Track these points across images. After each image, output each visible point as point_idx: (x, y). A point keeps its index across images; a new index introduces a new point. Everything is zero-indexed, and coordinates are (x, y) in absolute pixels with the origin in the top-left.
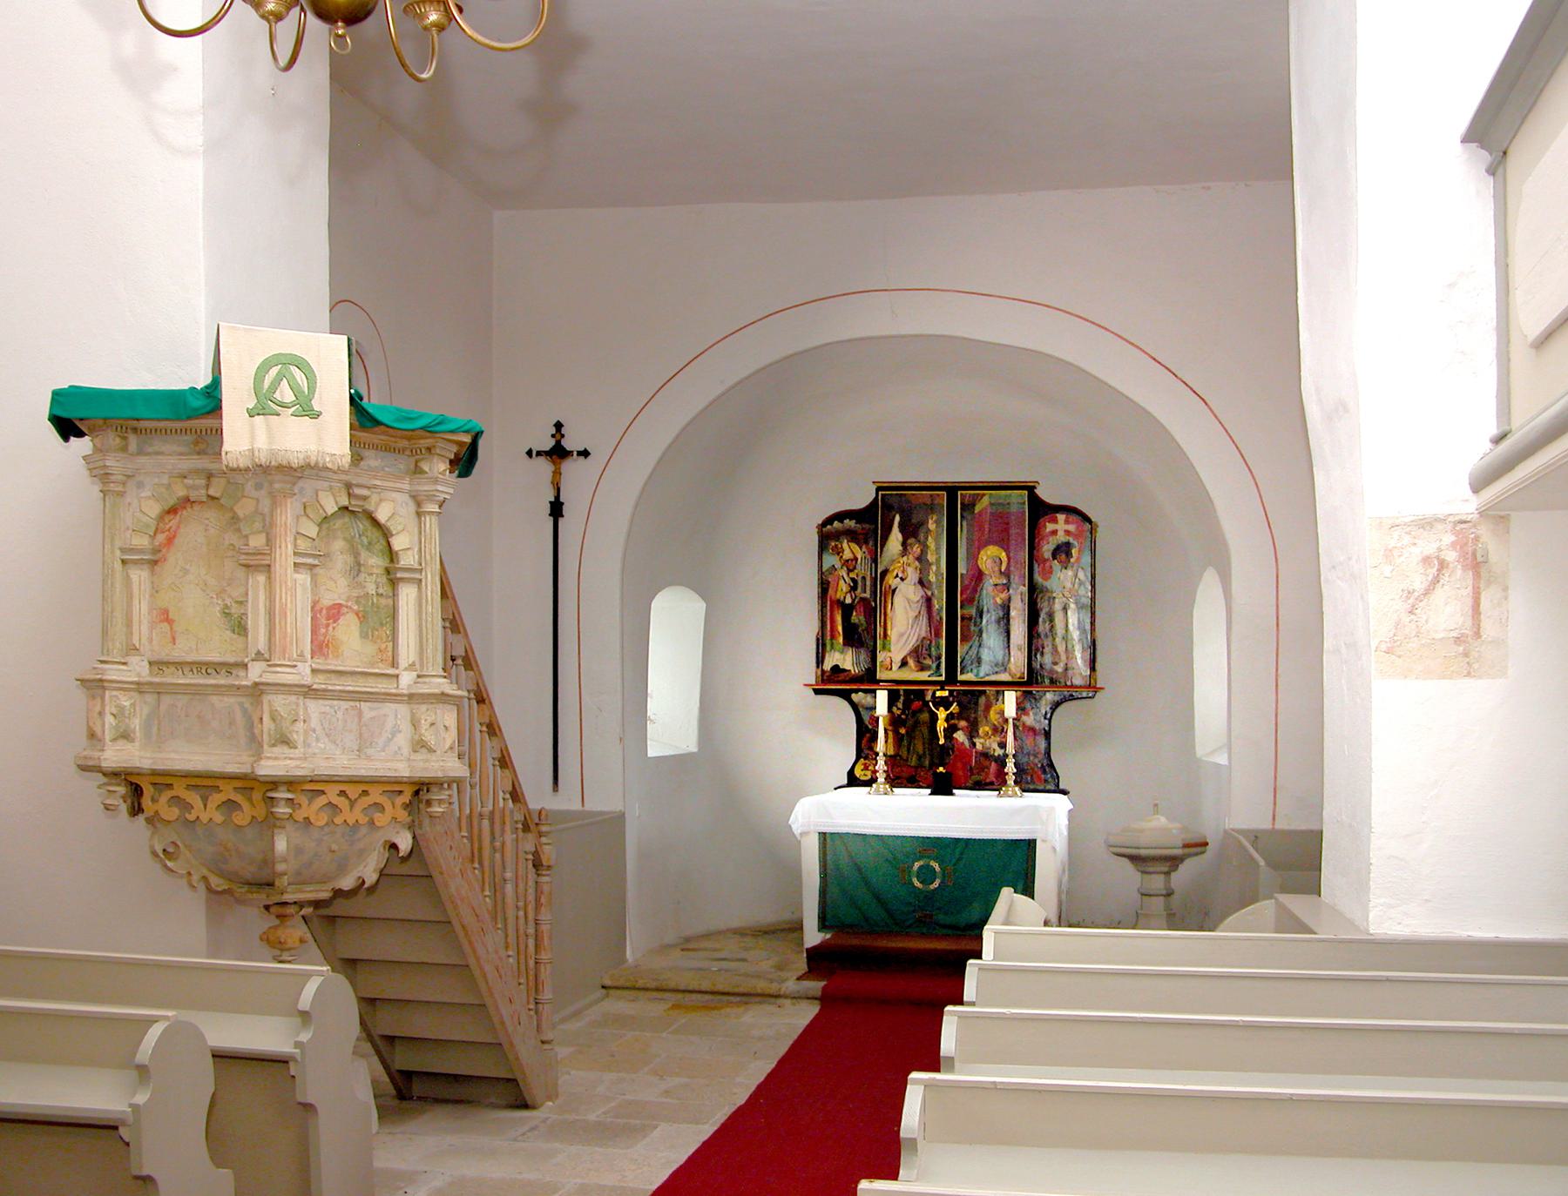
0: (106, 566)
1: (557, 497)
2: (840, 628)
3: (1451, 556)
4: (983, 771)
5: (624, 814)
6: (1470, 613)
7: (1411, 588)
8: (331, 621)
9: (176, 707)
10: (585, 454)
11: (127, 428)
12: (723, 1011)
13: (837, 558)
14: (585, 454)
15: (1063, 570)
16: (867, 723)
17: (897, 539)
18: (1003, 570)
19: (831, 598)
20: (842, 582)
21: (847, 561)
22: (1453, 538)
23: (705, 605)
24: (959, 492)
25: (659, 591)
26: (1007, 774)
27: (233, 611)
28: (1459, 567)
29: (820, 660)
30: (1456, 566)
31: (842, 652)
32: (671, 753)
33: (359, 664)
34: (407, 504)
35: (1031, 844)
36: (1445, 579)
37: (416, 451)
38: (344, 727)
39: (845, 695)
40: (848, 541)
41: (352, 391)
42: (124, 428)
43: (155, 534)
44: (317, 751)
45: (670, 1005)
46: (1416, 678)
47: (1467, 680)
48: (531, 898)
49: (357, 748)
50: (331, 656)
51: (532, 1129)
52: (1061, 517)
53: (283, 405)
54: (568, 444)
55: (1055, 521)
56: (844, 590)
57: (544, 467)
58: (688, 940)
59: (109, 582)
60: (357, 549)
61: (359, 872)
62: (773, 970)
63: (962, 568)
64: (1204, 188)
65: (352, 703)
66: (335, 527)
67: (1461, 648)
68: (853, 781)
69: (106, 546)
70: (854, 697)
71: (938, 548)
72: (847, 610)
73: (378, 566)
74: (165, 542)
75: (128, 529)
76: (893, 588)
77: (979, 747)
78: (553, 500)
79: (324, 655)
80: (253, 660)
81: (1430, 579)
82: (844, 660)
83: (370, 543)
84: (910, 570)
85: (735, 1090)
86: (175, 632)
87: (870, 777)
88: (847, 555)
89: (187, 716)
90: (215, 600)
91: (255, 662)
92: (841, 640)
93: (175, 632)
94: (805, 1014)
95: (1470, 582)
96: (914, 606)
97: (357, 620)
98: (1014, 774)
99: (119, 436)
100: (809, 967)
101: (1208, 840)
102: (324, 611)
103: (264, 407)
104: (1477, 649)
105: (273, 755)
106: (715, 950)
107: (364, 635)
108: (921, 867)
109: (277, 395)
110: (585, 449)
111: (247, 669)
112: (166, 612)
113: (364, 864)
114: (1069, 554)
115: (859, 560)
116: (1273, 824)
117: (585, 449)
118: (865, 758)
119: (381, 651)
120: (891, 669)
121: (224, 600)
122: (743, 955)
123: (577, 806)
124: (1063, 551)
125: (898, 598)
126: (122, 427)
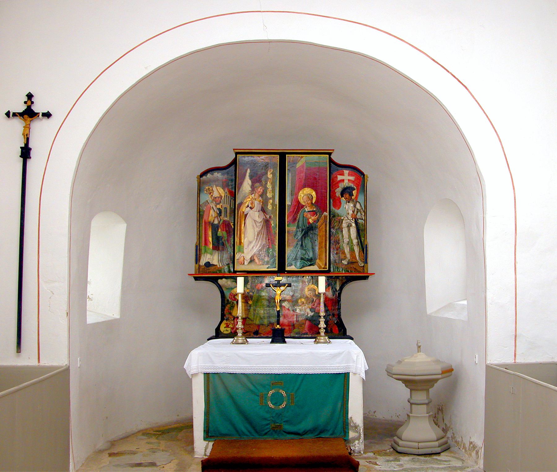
1: (27, 144)
2: (210, 239)
5: (69, 367)
10: (47, 115)
13: (210, 196)
14: (47, 115)
15: (348, 203)
17: (248, 184)
18: (313, 202)
19: (205, 220)
20: (212, 212)
21: (216, 198)
23: (126, 225)
24: (287, 155)
25: (92, 220)
26: (320, 328)
29: (197, 260)
31: (211, 254)
32: (103, 320)
39: (214, 280)
40: (216, 186)
52: (346, 172)
54: (36, 108)
55: (342, 174)
56: (213, 215)
57: (18, 124)
58: (113, 443)
63: (288, 202)
68: (218, 334)
70: (220, 281)
71: (273, 188)
72: (215, 228)
76: (245, 213)
78: (23, 146)
82: (213, 259)
84: (256, 203)
87: (230, 331)
88: (216, 194)
92: (211, 246)
96: (258, 224)
98: (324, 328)
108: (273, 395)
114: (351, 195)
115: (223, 197)
116: (515, 359)
118: (227, 320)
120: (244, 264)
123: (33, 362)
124: (347, 191)
125: (248, 220)
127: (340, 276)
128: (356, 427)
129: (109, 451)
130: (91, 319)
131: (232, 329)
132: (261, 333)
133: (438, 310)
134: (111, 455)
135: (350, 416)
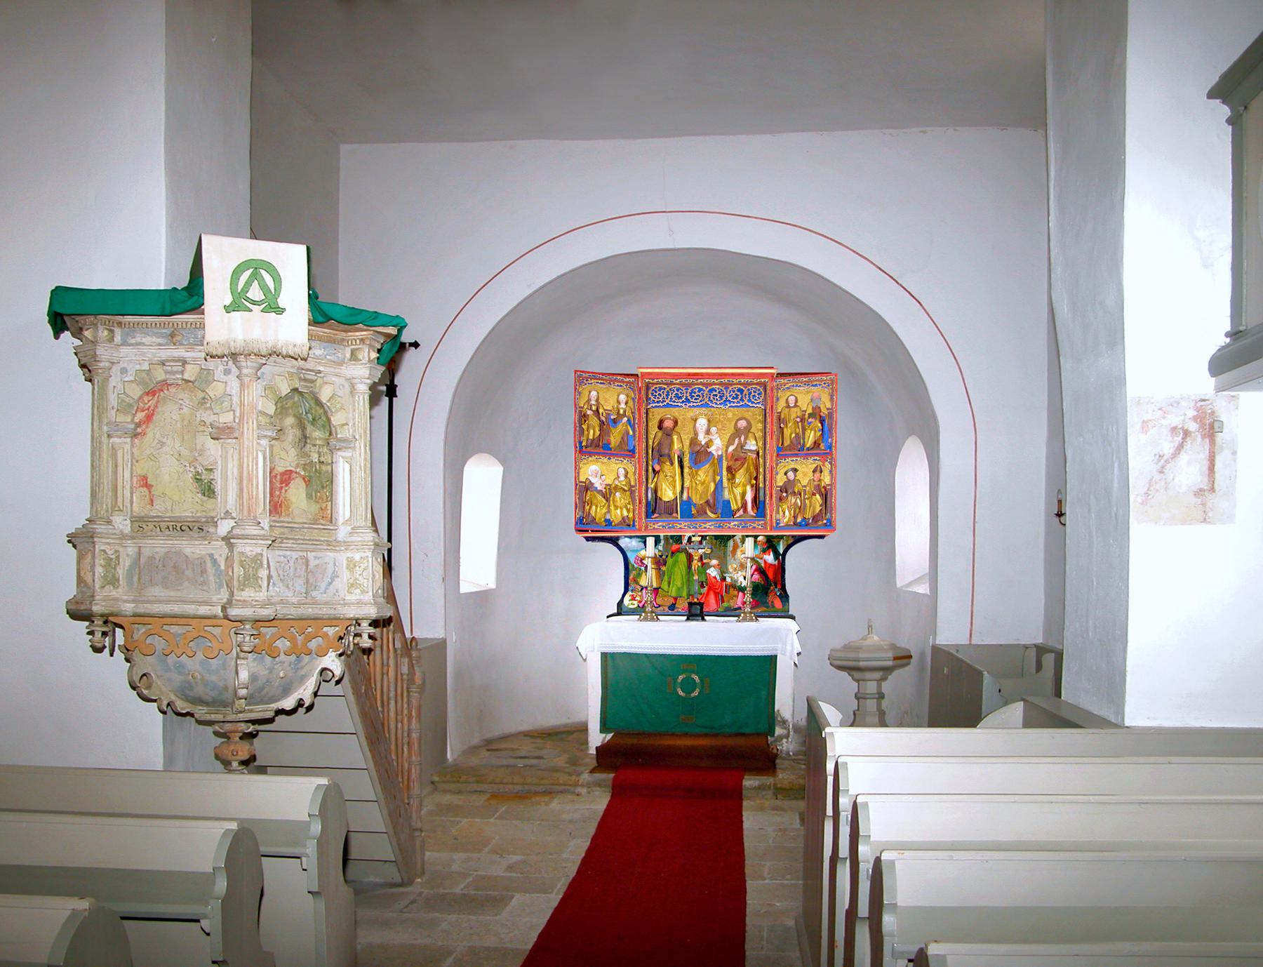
0: (95, 440)
3: (1193, 427)
4: (732, 599)
5: (446, 640)
6: (1207, 472)
7: (1161, 453)
8: (284, 485)
9: (155, 558)
10: (416, 345)
11: (113, 323)
12: (533, 800)
14: (416, 345)
16: (633, 563)
22: (1195, 413)
23: (502, 468)
27: (203, 477)
28: (1199, 436)
30: (1197, 435)
33: (305, 521)
34: (343, 386)
35: (773, 659)
36: (1188, 446)
37: (352, 342)
38: (295, 574)
39: (614, 541)
41: (311, 292)
42: (111, 322)
43: (136, 413)
44: (273, 594)
45: (488, 796)
46: (1164, 524)
47: (1204, 526)
48: (405, 712)
49: (304, 591)
50: (283, 514)
51: (413, 902)
53: (254, 303)
59: (98, 453)
60: (304, 424)
61: (299, 694)
62: (568, 765)
64: (920, 132)
65: (301, 554)
66: (287, 406)
67: (1200, 500)
69: (95, 423)
73: (320, 439)
74: (144, 419)
75: (113, 408)
77: (728, 580)
79: (278, 513)
80: (222, 519)
81: (1176, 446)
83: (314, 419)
85: (564, 865)
86: (153, 495)
89: (164, 566)
90: (188, 468)
91: (223, 520)
93: (153, 495)
94: (600, 801)
95: (1207, 447)
97: (304, 484)
99: (107, 329)
100: (598, 762)
101: (912, 654)
102: (279, 477)
103: (238, 304)
104: (1211, 501)
105: (242, 599)
106: (513, 750)
107: (309, 497)
109: (250, 295)
110: (416, 341)
111: (217, 526)
112: (145, 478)
113: (304, 687)
117: (416, 341)
119: (322, 509)
121: (195, 468)
122: (538, 753)
126: (109, 322)
127: (786, 535)
128: (784, 722)
129: (487, 748)
130: (465, 588)
131: (640, 602)
132: (678, 608)
133: (910, 584)
134: (488, 750)
135: (776, 708)
